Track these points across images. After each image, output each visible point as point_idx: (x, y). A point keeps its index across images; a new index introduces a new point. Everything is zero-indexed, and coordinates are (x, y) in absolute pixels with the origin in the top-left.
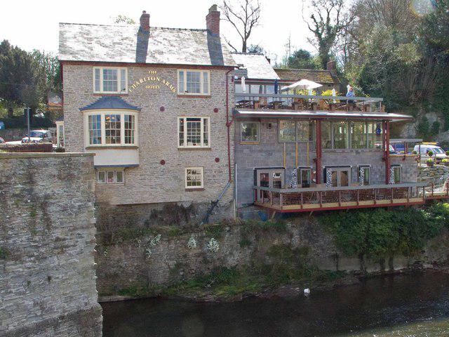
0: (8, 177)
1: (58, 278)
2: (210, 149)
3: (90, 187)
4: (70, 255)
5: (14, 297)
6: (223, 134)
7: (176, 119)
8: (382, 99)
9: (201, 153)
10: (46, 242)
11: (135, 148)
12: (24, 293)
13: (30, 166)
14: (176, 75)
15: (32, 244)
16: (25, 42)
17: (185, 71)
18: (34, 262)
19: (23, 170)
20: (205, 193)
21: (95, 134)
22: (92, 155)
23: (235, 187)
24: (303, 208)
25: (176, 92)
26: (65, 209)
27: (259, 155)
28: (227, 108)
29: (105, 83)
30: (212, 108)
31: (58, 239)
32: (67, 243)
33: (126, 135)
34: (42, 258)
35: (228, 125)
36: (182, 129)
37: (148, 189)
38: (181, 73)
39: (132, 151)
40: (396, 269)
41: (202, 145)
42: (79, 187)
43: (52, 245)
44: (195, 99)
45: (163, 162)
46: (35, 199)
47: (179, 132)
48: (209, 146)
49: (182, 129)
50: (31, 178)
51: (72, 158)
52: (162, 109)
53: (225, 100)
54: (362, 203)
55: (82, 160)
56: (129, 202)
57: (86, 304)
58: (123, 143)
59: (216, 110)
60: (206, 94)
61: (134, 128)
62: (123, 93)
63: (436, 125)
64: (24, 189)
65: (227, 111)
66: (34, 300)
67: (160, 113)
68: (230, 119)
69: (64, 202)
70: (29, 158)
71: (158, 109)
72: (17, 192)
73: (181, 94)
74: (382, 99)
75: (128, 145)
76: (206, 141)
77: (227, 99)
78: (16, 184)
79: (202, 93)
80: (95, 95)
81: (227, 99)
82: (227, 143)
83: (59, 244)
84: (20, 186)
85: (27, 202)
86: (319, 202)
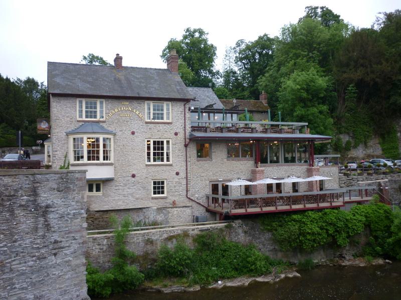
0: (16, 191)
1: (55, 274)
2: (171, 165)
3: (83, 198)
4: (66, 254)
5: (18, 292)
7: (144, 141)
8: (307, 124)
9: (164, 168)
10: (46, 244)
11: (111, 164)
12: (26, 288)
13: (34, 182)
15: (35, 246)
16: (16, 73)
18: (35, 261)
19: (29, 184)
20: (168, 201)
22: (85, 172)
23: (237, 131)
24: (278, 209)
25: (144, 119)
26: (62, 217)
28: (185, 132)
29: (87, 112)
30: (173, 132)
31: (56, 242)
32: (63, 244)
33: (104, 153)
34: (42, 258)
35: (186, 146)
37: (121, 197)
39: (109, 167)
40: (316, 261)
42: (74, 198)
43: (51, 247)
44: (159, 125)
45: (134, 176)
46: (37, 207)
47: (146, 151)
48: (170, 121)
50: (35, 191)
51: (69, 174)
52: (133, 133)
53: (183, 126)
54: (295, 207)
55: (77, 175)
56: (106, 208)
57: (78, 296)
58: (101, 160)
59: (176, 134)
60: (168, 121)
61: (110, 148)
62: (101, 119)
63: (348, 143)
64: (30, 201)
65: (185, 134)
66: (35, 295)
69: (62, 210)
70: (33, 175)
71: (130, 132)
72: (23, 203)
73: (149, 121)
74: (307, 124)
75: (106, 162)
76: (168, 160)
77: (185, 125)
78: (22, 196)
79: (165, 120)
81: (185, 125)
83: (56, 246)
84: (25, 197)
85: (31, 211)
86: (260, 207)
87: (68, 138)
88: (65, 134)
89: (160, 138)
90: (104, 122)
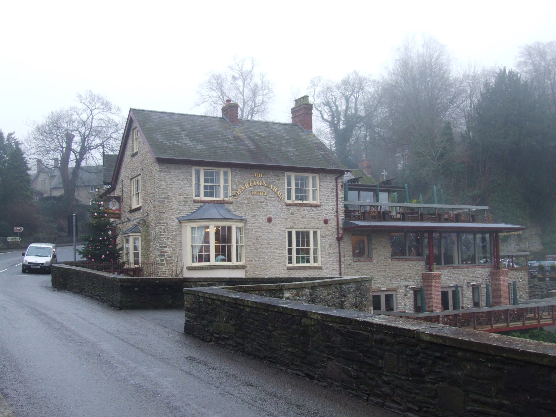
6: (334, 249)
14: (284, 180)
17: (293, 176)
21: (303, 241)
27: (194, 373)
36: (290, 243)
38: (198, 173)
41: (312, 264)
44: (303, 208)
49: (290, 243)
52: (270, 220)
53: (335, 209)
60: (315, 202)
62: (226, 199)
65: (338, 222)
67: (268, 225)
68: (341, 231)
71: (265, 219)
79: (310, 201)
80: (195, 201)
82: (338, 259)
87: (181, 227)
88: (177, 221)
89: (305, 228)
90: (230, 203)
